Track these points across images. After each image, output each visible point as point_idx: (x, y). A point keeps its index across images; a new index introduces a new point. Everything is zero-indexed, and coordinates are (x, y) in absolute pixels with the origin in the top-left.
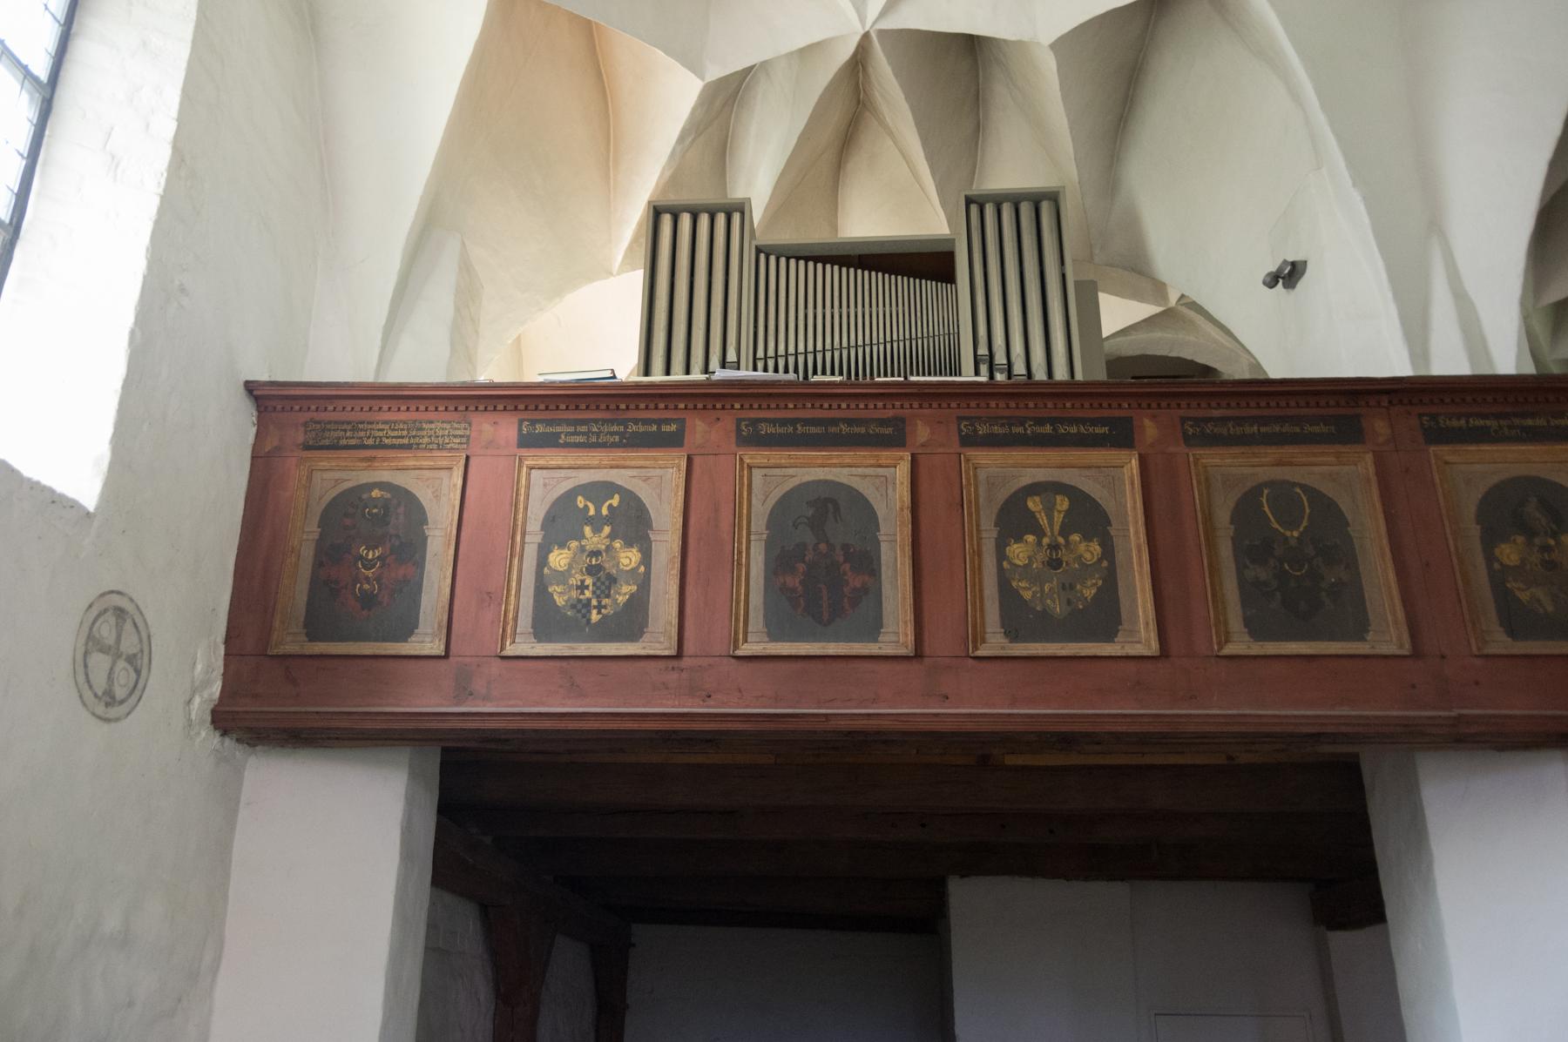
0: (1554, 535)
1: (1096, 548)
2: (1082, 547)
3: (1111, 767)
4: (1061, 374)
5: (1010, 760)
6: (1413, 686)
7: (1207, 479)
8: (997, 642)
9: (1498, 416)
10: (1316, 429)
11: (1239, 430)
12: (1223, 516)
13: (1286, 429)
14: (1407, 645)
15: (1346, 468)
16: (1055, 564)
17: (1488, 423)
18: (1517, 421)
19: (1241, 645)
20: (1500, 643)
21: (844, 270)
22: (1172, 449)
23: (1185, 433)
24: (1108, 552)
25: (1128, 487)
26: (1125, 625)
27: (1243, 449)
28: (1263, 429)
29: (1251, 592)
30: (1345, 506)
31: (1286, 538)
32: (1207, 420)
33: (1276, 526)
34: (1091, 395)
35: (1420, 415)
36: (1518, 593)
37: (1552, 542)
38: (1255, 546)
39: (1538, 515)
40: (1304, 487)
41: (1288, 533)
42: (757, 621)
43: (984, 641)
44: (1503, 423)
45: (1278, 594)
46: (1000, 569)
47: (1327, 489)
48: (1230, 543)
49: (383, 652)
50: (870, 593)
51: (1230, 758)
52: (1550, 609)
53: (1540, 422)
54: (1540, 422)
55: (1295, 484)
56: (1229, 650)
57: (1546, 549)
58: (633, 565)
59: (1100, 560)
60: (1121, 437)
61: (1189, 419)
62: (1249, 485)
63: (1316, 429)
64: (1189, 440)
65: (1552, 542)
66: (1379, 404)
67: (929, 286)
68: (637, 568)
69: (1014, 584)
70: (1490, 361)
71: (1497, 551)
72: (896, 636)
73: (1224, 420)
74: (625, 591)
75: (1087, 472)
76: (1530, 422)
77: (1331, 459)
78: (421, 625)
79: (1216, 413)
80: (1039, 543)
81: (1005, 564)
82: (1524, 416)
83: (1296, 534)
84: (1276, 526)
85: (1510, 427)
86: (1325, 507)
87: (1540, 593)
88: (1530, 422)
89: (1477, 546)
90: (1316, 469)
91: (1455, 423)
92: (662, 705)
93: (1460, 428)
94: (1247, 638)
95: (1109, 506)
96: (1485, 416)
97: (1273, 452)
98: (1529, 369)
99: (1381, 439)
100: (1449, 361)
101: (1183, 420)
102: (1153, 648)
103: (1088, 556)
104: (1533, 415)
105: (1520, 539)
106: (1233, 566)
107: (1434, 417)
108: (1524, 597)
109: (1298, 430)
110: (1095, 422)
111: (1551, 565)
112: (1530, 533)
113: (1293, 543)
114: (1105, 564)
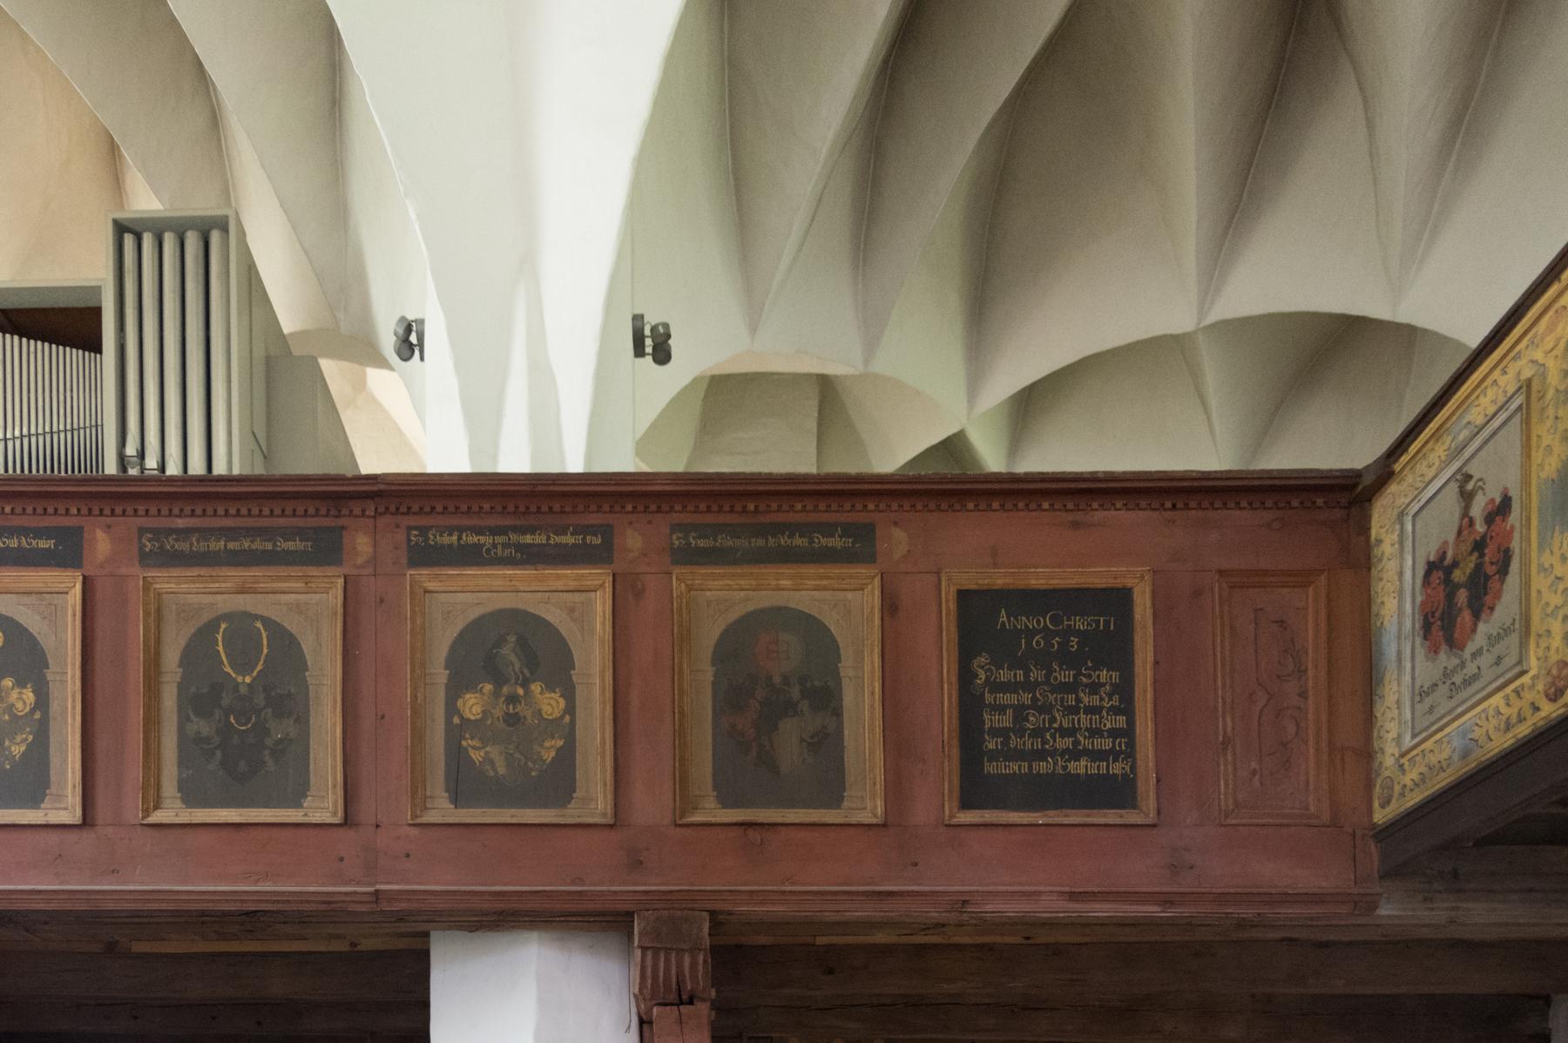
0: (525, 684)
1: (29, 696)
2: (14, 695)
3: (167, 955)
4: (173, 469)
5: (139, 947)
6: (342, 859)
7: (159, 610)
8: (442, 810)
9: (495, 531)
10: (290, 546)
11: (203, 546)
12: (171, 657)
13: (258, 545)
14: (340, 814)
15: (317, 596)
16: (513, 720)
17: (482, 539)
18: (514, 537)
19: (171, 812)
20: (442, 810)
21: (16, 338)
22: (123, 571)
23: (141, 547)
24: (42, 702)
25: (70, 619)
26: (53, 790)
27: (203, 571)
28: (231, 545)
29: (190, 747)
30: (307, 646)
31: (237, 686)
32: (170, 531)
33: (228, 669)
34: (21, 495)
35: (410, 528)
36: (472, 753)
37: (521, 691)
38: (203, 696)
39: (513, 658)
40: (266, 621)
41: (240, 679)
42: (169, 787)
43: (157, 807)
44: (499, 539)
45: (218, 753)
46: (448, 722)
47: (292, 624)
48: (175, 691)
49: (780, 820)
50: (295, 752)
51: (353, 944)
52: (502, 770)
53: (539, 539)
54: (539, 539)
55: (257, 617)
56: (158, 817)
57: (512, 699)
58: (557, 714)
59: (33, 711)
60: (68, 553)
61: (416, 528)
62: (206, 617)
63: (290, 546)
64: (145, 559)
65: (521, 691)
66: (363, 514)
67: (74, 355)
68: (562, 717)
69: (464, 743)
70: (356, 465)
71: (460, 703)
72: (323, 806)
73: (185, 533)
74: (549, 750)
75: (26, 599)
76: (528, 539)
77: (300, 585)
78: (312, 788)
79: (180, 523)
80: (496, 694)
81: (456, 720)
82: (523, 530)
83: (248, 680)
84: (228, 669)
85: (505, 546)
86: (285, 643)
87: (494, 752)
88: (528, 539)
89: (441, 695)
90: (283, 598)
91: (445, 540)
92: (142, 883)
93: (450, 546)
94: (179, 803)
95: (47, 642)
96: (479, 531)
97: (234, 575)
98: (259, 470)
99: (360, 561)
100: (515, 459)
101: (142, 531)
102: (72, 815)
103: (20, 705)
104: (532, 530)
105: (488, 687)
106: (175, 717)
107: (424, 531)
108: (476, 756)
109: (269, 546)
110: (39, 533)
111: (513, 720)
112: (499, 679)
113: (243, 690)
114: (37, 716)
